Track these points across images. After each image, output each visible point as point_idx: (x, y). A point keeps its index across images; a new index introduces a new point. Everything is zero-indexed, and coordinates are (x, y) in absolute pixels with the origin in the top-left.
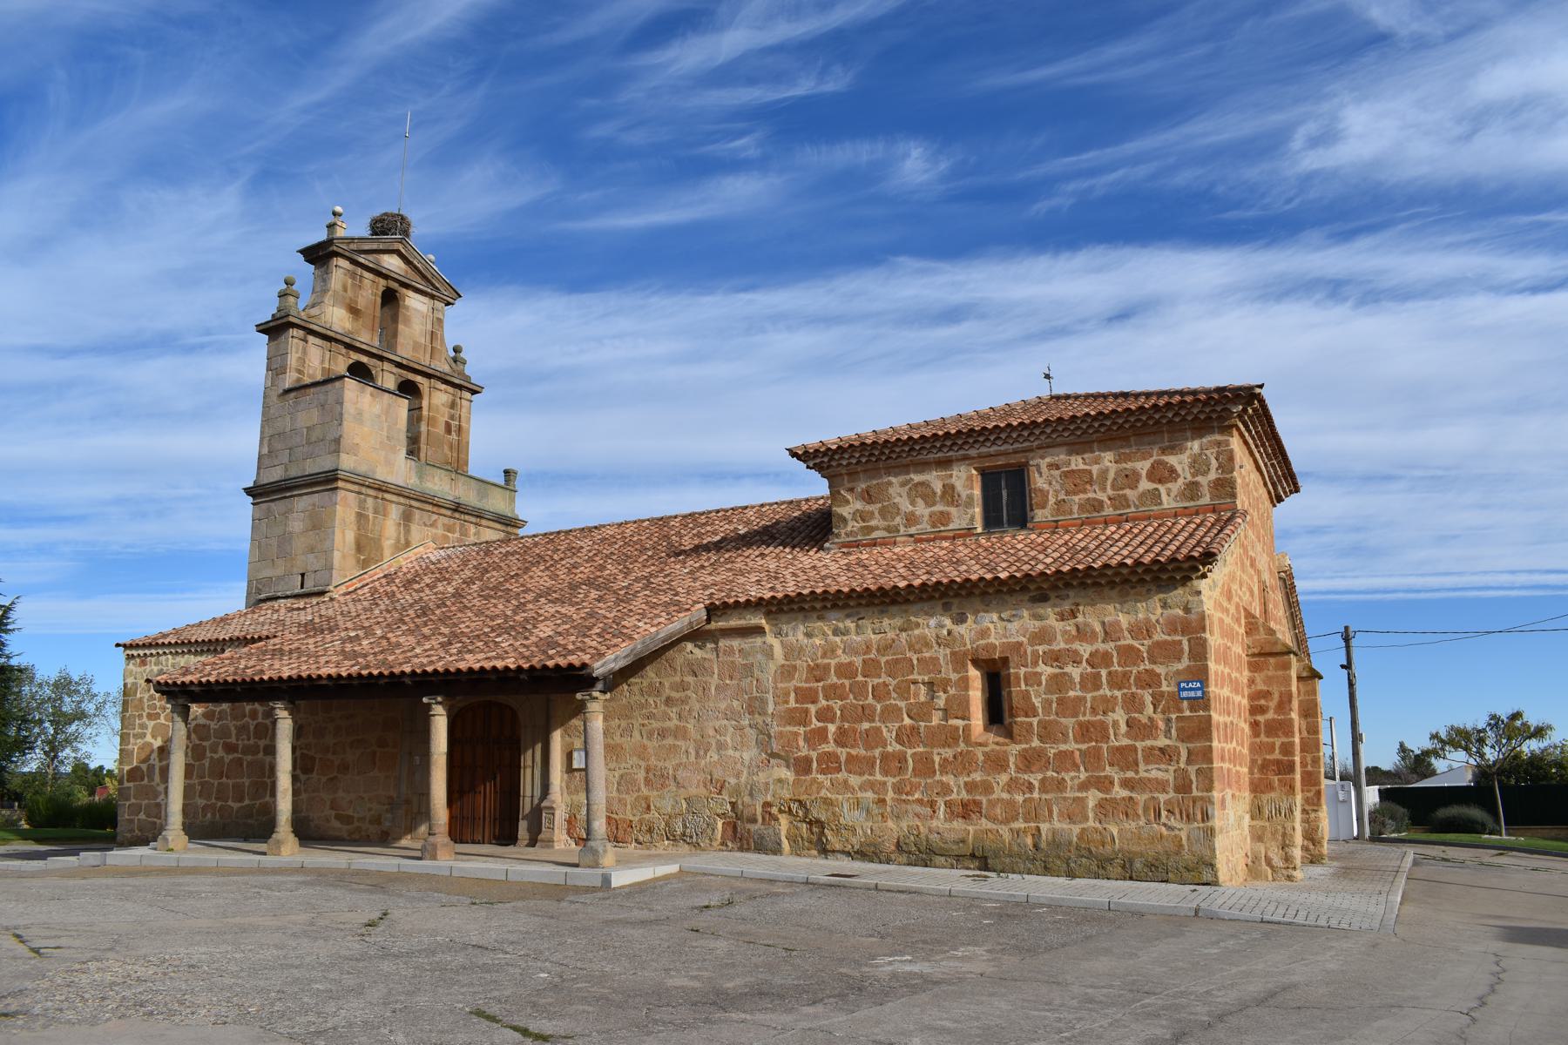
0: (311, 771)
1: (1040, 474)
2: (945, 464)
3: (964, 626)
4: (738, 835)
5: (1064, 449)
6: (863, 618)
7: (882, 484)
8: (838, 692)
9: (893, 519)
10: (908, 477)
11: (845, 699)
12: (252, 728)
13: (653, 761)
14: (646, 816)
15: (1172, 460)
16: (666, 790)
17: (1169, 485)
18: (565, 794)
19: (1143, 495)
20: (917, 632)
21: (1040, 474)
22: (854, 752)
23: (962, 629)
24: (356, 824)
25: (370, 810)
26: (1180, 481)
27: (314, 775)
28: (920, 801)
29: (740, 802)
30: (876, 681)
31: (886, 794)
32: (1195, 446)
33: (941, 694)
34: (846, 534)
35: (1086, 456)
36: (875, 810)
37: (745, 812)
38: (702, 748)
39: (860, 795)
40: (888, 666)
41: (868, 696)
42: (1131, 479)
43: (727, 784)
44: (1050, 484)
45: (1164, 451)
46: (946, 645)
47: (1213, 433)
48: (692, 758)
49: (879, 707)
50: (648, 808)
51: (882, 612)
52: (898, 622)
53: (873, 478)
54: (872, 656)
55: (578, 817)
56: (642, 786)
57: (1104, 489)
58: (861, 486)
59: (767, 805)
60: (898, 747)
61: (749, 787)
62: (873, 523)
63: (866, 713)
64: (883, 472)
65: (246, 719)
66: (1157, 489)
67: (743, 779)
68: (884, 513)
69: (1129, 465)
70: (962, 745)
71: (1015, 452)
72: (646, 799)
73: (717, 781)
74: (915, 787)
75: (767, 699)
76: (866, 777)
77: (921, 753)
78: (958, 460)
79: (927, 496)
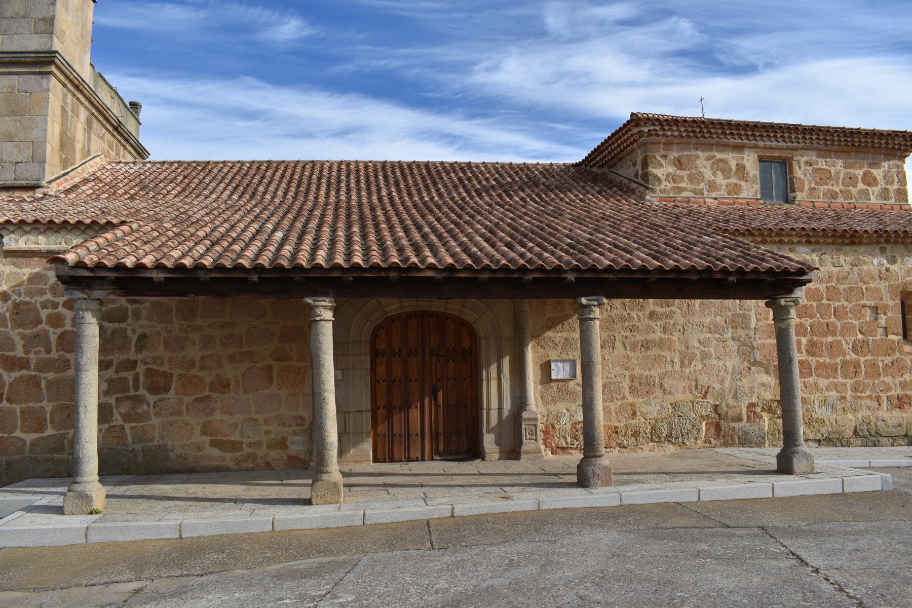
0: (167, 389)
1: (800, 167)
2: (739, 148)
3: (896, 265)
4: (722, 433)
5: (815, 153)
6: (825, 254)
7: (691, 155)
8: (809, 312)
9: (699, 184)
10: (711, 154)
11: (814, 317)
12: (53, 338)
13: (638, 371)
14: (633, 422)
15: (874, 172)
16: (652, 396)
17: (873, 188)
18: (540, 404)
19: (859, 192)
20: (865, 267)
21: (800, 167)
22: (821, 360)
23: (894, 268)
24: (246, 450)
25: (267, 433)
26: (879, 186)
27: (172, 394)
28: (870, 397)
29: (724, 404)
30: (837, 304)
31: (847, 393)
32: (886, 165)
33: (882, 315)
34: (660, 191)
35: (827, 160)
36: (839, 405)
37: (730, 413)
38: (686, 359)
39: (827, 394)
40: (845, 293)
41: (831, 315)
42: (852, 180)
43: (711, 389)
44: (805, 175)
45: (871, 165)
46: (886, 279)
47: (895, 159)
48: (677, 367)
49: (839, 324)
50: (634, 414)
51: (838, 250)
52: (850, 259)
53: (683, 150)
54: (833, 284)
55: (557, 427)
56: (627, 394)
57: (838, 185)
58: (674, 154)
59: (751, 406)
60: (854, 356)
61: (733, 391)
62: (682, 185)
63: (829, 329)
64: (692, 146)
65: (44, 325)
66: (867, 190)
67: (727, 384)
68: (691, 178)
69: (852, 171)
70: (898, 354)
71: (787, 149)
72: (632, 405)
73: (703, 386)
74: (866, 387)
75: (749, 316)
76: (831, 380)
77: (870, 360)
78: (750, 147)
79: (726, 170)
